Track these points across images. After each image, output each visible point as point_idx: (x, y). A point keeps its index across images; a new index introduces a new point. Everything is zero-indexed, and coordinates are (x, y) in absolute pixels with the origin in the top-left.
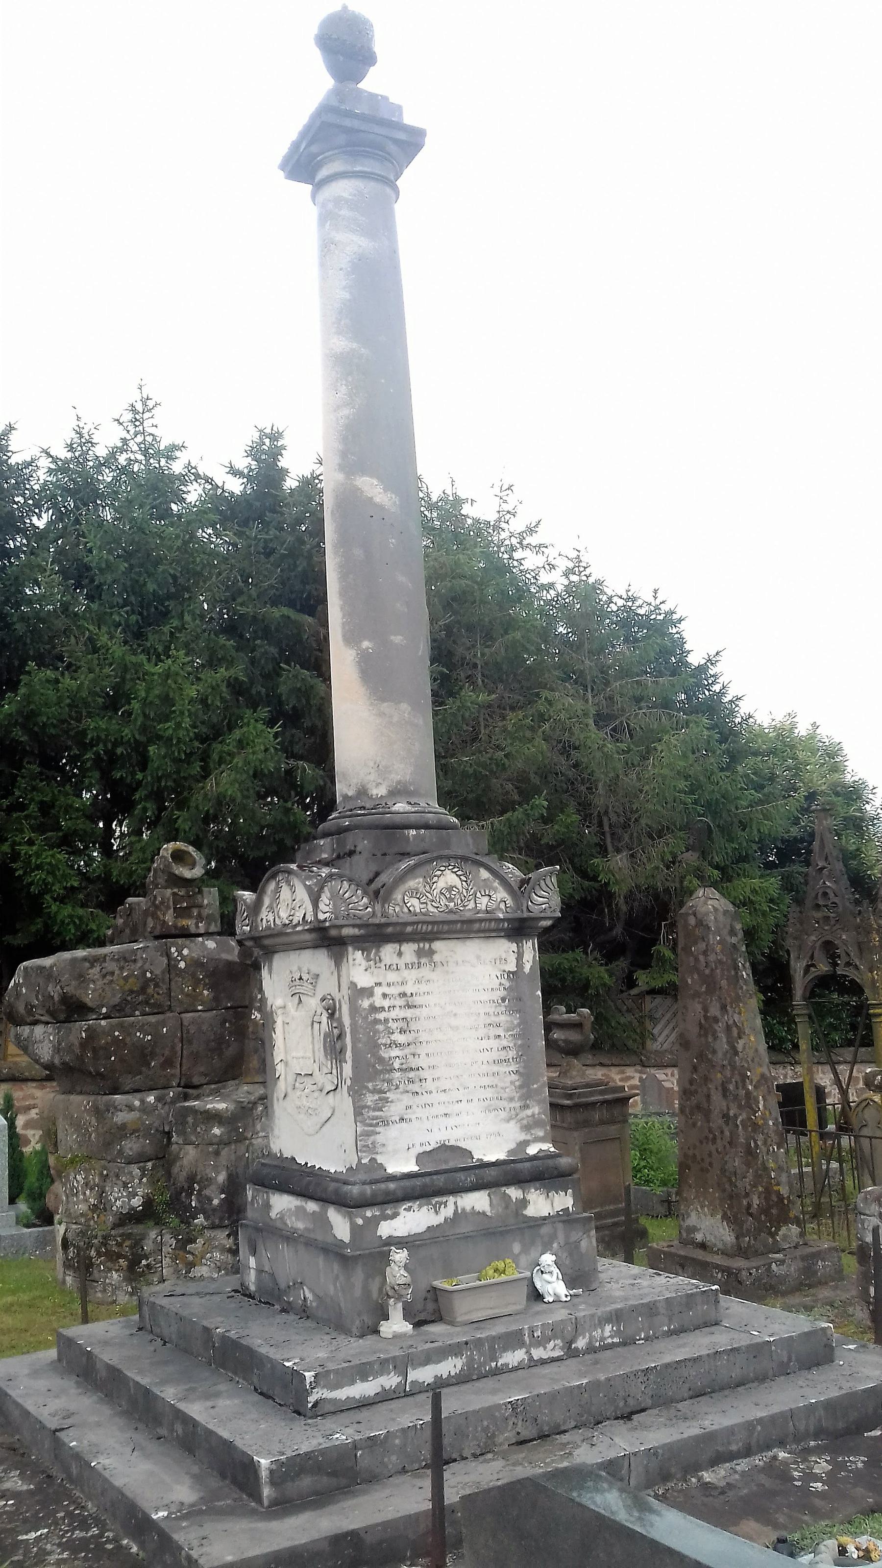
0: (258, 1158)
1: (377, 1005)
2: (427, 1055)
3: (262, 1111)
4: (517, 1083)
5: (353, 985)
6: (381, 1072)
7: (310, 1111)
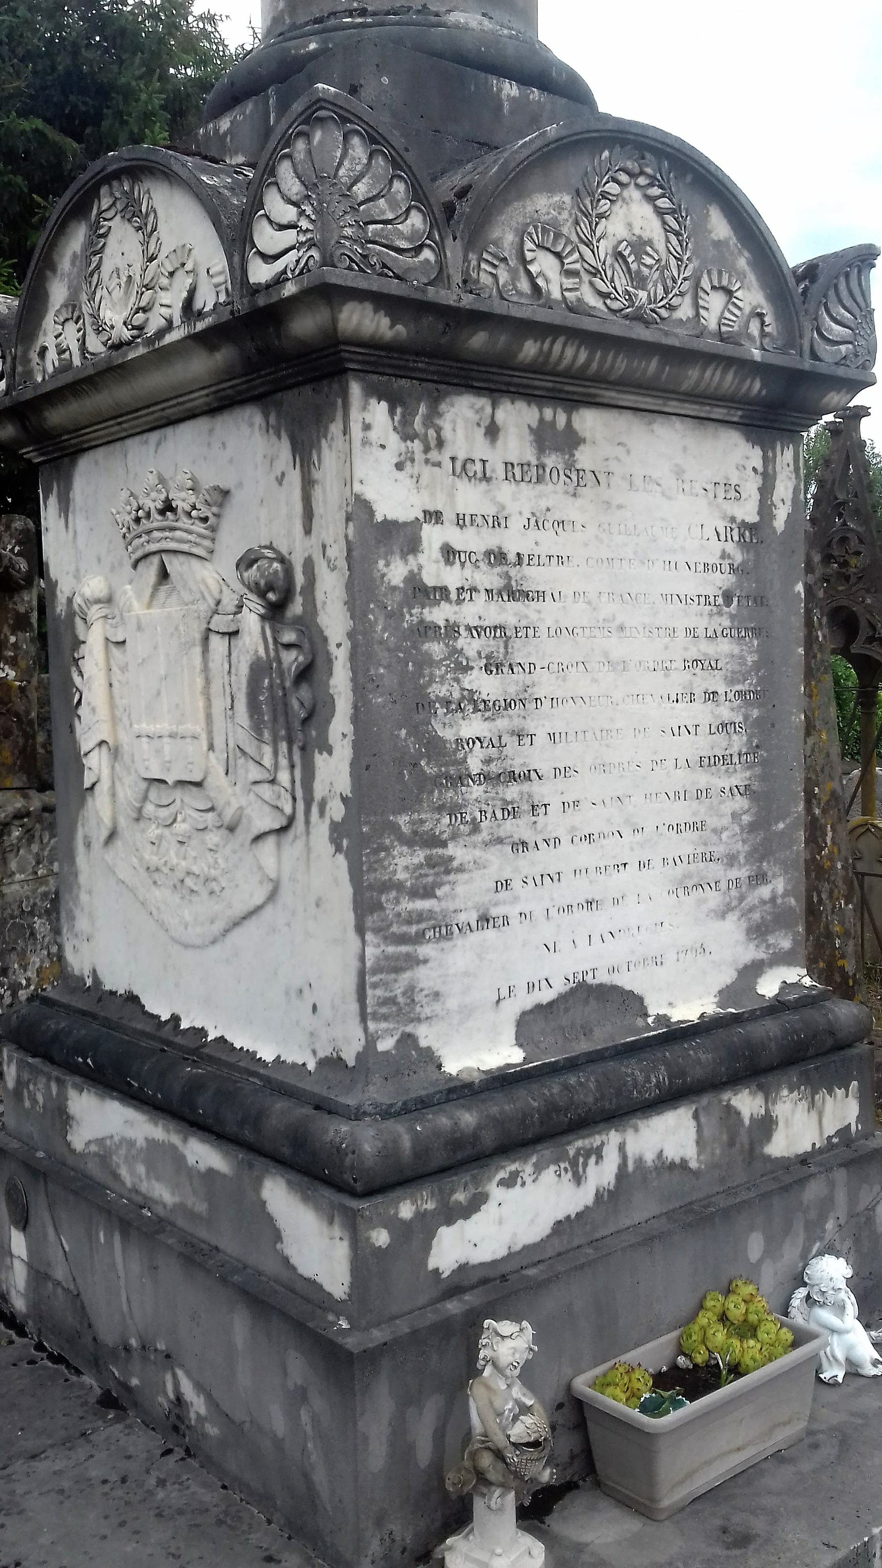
0: (12, 917)
1: (429, 580)
2: (552, 736)
3: (20, 839)
4: (746, 819)
5: (360, 509)
6: (435, 781)
7: (189, 882)
